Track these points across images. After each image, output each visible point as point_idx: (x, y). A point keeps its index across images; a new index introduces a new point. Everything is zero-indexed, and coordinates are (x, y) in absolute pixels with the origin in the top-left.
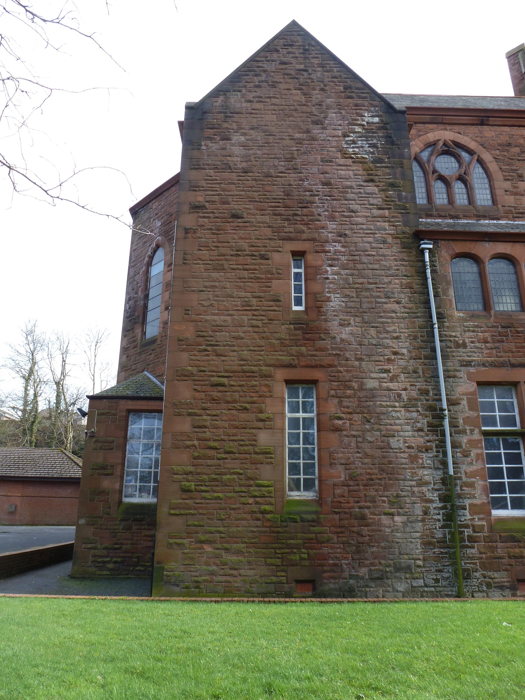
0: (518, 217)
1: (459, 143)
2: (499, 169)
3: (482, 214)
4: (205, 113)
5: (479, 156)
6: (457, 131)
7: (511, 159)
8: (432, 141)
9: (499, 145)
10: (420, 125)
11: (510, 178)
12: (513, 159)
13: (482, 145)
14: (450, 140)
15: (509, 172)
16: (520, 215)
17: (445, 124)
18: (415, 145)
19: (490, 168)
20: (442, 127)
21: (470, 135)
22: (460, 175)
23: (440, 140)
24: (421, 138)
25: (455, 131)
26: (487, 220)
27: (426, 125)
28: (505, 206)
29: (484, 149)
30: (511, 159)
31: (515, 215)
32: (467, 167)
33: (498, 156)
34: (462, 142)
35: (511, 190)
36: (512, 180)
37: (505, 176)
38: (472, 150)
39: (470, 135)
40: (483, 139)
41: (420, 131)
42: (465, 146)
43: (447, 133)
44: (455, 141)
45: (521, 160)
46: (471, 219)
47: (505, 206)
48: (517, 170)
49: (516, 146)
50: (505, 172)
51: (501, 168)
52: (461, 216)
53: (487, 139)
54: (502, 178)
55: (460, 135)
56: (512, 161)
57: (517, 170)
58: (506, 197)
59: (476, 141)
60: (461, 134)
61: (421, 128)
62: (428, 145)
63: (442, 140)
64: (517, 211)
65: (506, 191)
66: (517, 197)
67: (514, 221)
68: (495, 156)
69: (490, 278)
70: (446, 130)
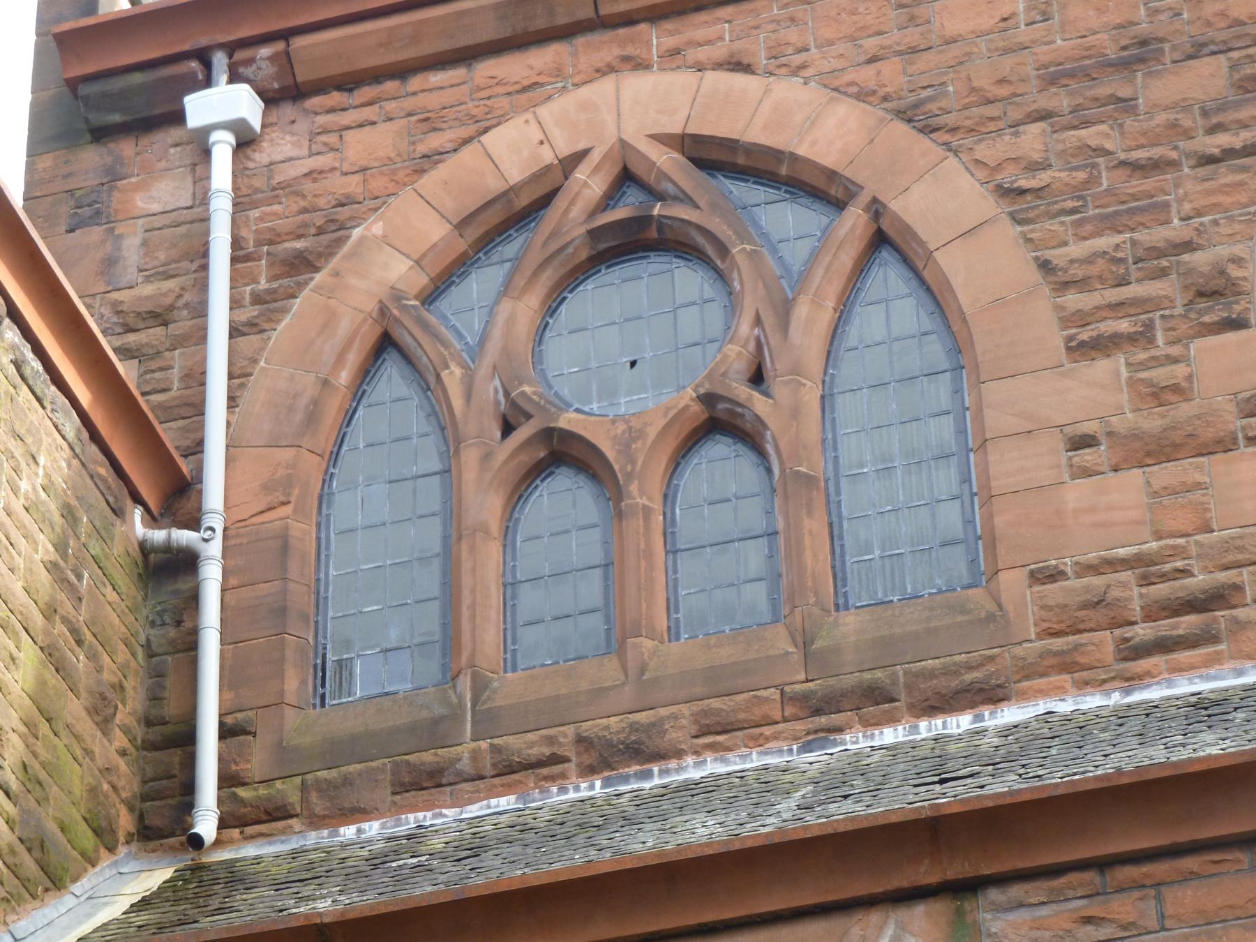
0: (1163, 646)
1: (730, 145)
2: (1035, 276)
3: (849, 680)
4: (102, 273)
5: (876, 209)
6: (719, 52)
7: (1137, 168)
8: (515, 175)
9: (1053, 78)
10: (436, 78)
11: (1124, 326)
12: (1156, 166)
13: (906, 115)
14: (663, 139)
15: (1123, 282)
16: (1188, 623)
17: (628, 20)
18: (385, 240)
19: (957, 282)
20: (602, 47)
21: (820, 61)
22: (709, 399)
23: (579, 157)
24: (430, 182)
25: (702, 54)
26: (892, 720)
27: (487, 69)
28: (1055, 575)
29: (925, 143)
30: (1137, 168)
31: (1143, 632)
32: (769, 320)
33: (1034, 167)
34: (756, 134)
35: (1127, 420)
36: (1144, 336)
37: (1082, 319)
38: (832, 175)
39: (820, 61)
40: (924, 62)
41: (430, 123)
42: (777, 155)
43: (636, 85)
44: (698, 139)
45: (1229, 154)
46: (758, 742)
47: (1055, 575)
48: (1188, 246)
49: (1197, 50)
50: (1082, 284)
51: (1045, 266)
52: (675, 736)
53: (955, 51)
54: (1057, 339)
55: (740, 80)
56: (1150, 183)
57: (1188, 246)
58: (1076, 493)
59: (863, 95)
60: (747, 68)
61: (447, 97)
62: (494, 217)
63: (596, 156)
64: (1161, 590)
65: (1082, 442)
66: (1165, 474)
67: (1132, 681)
68: (1007, 177)
69: (406, 482)
70: (639, 65)
